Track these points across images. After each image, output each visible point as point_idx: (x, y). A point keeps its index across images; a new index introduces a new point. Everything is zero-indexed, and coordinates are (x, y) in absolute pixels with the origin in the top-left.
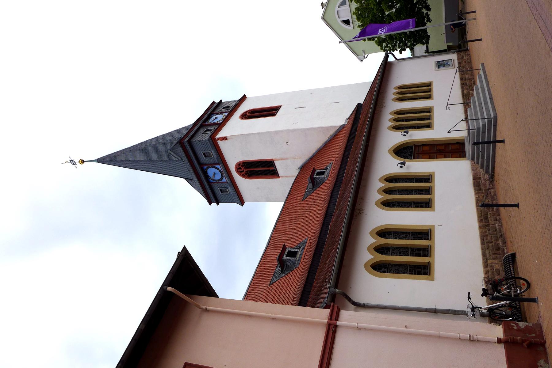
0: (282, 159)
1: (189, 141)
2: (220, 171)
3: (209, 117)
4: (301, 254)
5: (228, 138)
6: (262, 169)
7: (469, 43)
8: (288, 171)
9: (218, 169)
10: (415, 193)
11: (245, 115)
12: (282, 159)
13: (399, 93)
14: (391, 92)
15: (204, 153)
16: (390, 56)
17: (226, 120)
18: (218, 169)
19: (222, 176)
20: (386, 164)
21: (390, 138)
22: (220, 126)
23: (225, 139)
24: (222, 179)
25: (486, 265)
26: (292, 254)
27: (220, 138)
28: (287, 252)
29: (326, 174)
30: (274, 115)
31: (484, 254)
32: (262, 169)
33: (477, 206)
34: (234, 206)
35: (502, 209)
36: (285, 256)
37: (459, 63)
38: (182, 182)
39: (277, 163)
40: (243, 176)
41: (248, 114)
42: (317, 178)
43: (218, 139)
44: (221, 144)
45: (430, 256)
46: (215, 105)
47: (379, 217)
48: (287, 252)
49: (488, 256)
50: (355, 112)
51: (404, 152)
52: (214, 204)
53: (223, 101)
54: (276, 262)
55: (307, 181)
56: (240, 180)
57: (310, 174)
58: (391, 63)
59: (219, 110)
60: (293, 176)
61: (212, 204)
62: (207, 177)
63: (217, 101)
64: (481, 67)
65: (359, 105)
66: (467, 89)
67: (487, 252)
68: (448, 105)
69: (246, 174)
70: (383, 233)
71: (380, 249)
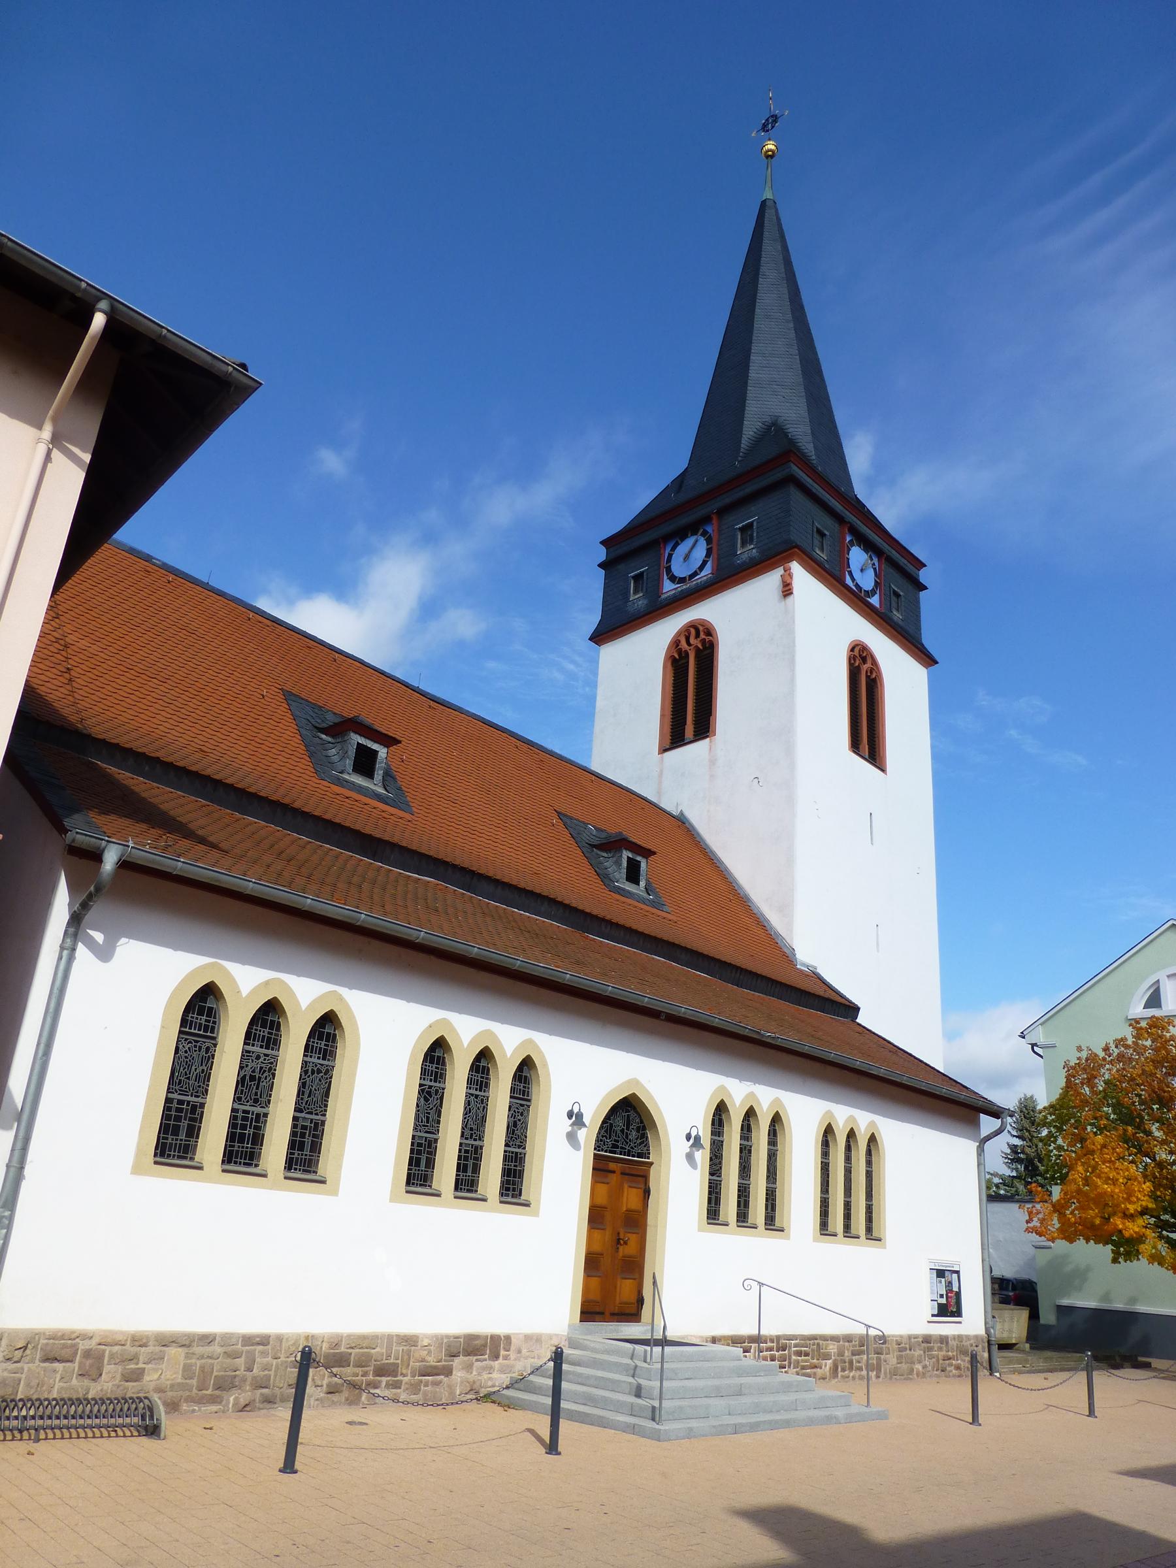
0: (713, 762)
1: (792, 480)
2: (695, 574)
3: (868, 546)
4: (360, 789)
5: (790, 599)
6: (690, 706)
7: (1085, 1373)
8: (681, 783)
9: (702, 568)
10: (464, 1143)
11: (864, 660)
12: (713, 762)
13: (851, 1135)
14: (851, 1114)
15: (751, 524)
16: (997, 1123)
17: (856, 599)
18: (702, 568)
19: (682, 580)
20: (583, 1071)
21: (682, 1092)
22: (833, 576)
23: (787, 590)
24: (673, 579)
25: (166, 1341)
26: (365, 763)
27: (790, 575)
28: (375, 746)
29: (629, 887)
30: (855, 746)
31: (207, 1339)
32: (690, 706)
33: (390, 1337)
34: (593, 619)
35: (286, 1413)
36: (362, 741)
37: (943, 1340)
38: (679, 462)
39: (703, 744)
40: (675, 643)
41: (865, 667)
42: (618, 863)
43: (788, 574)
44: (771, 581)
45: (156, 1163)
46: (910, 568)
47: (388, 1029)
48: (375, 746)
49: (198, 1350)
50: (829, 994)
51: (626, 1133)
52: (601, 554)
53: (922, 594)
54: (349, 713)
55: (616, 825)
56: (660, 636)
57: (633, 840)
58: (976, 1124)
59: (898, 584)
60: (659, 793)
61: (603, 550)
62: (681, 534)
63: (924, 576)
64: (874, 1409)
65: (851, 1010)
66: (841, 1354)
67: (216, 1349)
68: (761, 1284)
69: (680, 652)
70: (326, 1031)
71: (268, 1019)
